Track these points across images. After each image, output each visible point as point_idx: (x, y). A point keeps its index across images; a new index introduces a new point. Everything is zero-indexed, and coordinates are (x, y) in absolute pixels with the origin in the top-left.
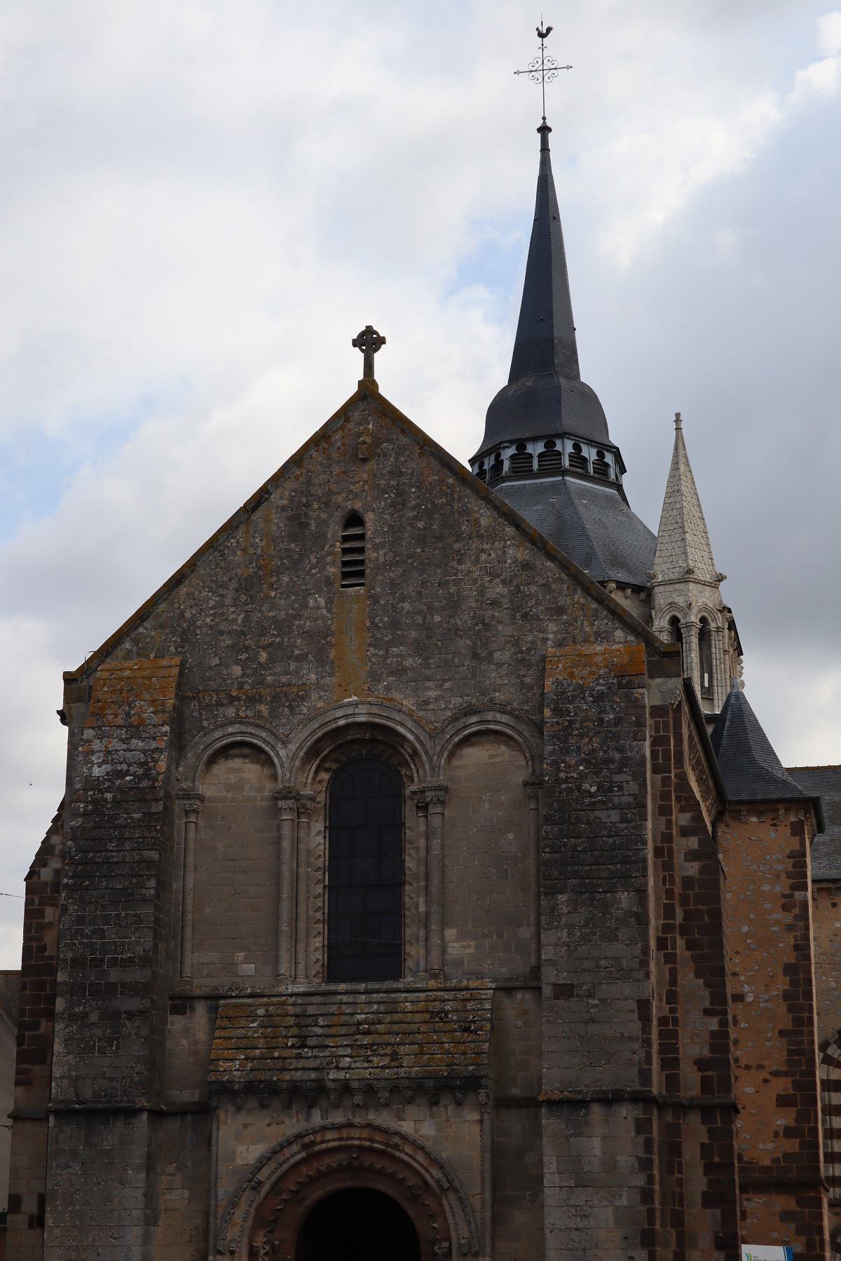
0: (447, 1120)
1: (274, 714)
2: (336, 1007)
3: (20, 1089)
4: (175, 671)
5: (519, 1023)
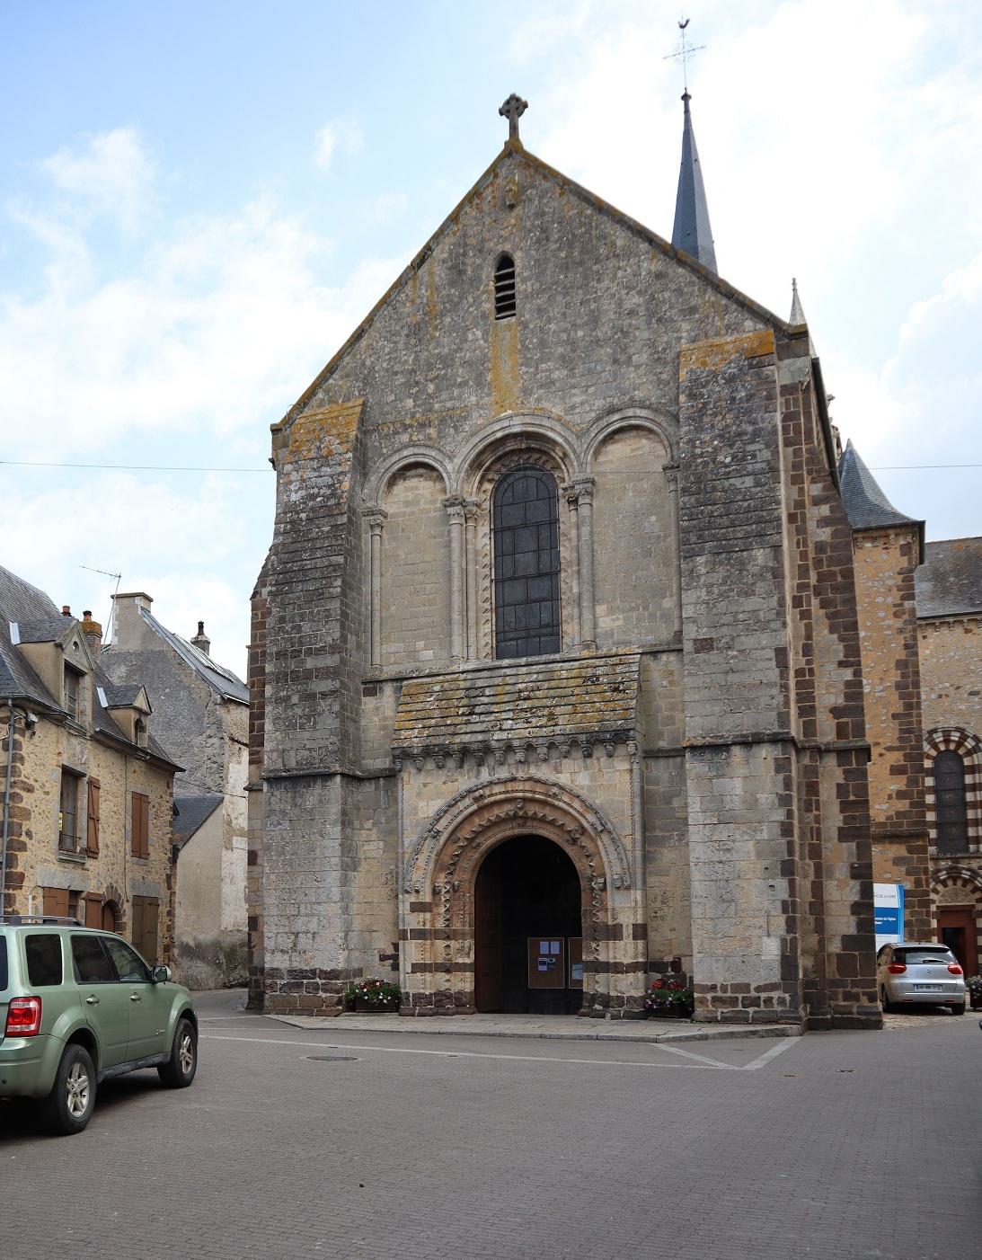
0: (600, 770)
1: (441, 435)
2: (501, 679)
3: (253, 766)
4: (359, 409)
5: (665, 683)
